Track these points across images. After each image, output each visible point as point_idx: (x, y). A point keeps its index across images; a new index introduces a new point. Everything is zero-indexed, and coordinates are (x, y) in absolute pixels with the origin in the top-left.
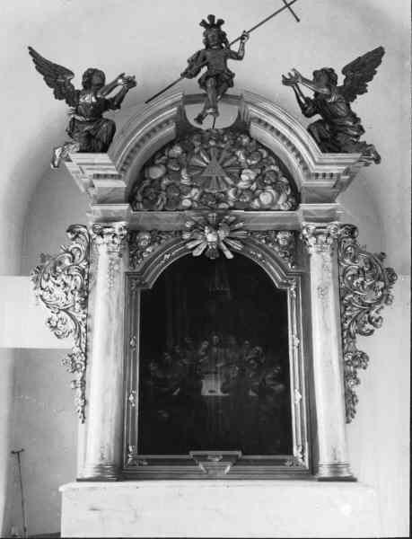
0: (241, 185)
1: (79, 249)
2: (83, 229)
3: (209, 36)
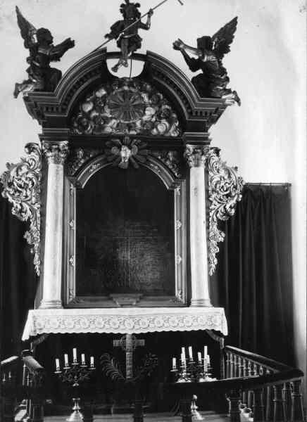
0: (145, 118)
1: (33, 160)
2: (36, 146)
3: (126, 11)
